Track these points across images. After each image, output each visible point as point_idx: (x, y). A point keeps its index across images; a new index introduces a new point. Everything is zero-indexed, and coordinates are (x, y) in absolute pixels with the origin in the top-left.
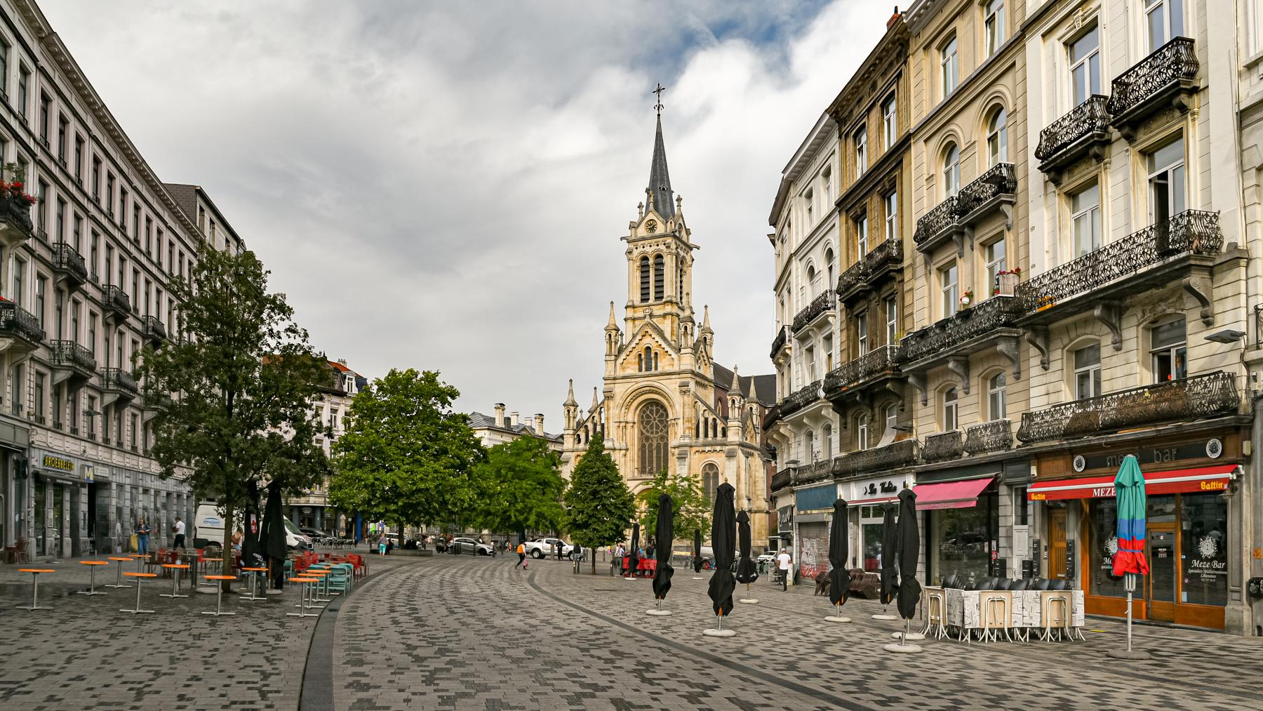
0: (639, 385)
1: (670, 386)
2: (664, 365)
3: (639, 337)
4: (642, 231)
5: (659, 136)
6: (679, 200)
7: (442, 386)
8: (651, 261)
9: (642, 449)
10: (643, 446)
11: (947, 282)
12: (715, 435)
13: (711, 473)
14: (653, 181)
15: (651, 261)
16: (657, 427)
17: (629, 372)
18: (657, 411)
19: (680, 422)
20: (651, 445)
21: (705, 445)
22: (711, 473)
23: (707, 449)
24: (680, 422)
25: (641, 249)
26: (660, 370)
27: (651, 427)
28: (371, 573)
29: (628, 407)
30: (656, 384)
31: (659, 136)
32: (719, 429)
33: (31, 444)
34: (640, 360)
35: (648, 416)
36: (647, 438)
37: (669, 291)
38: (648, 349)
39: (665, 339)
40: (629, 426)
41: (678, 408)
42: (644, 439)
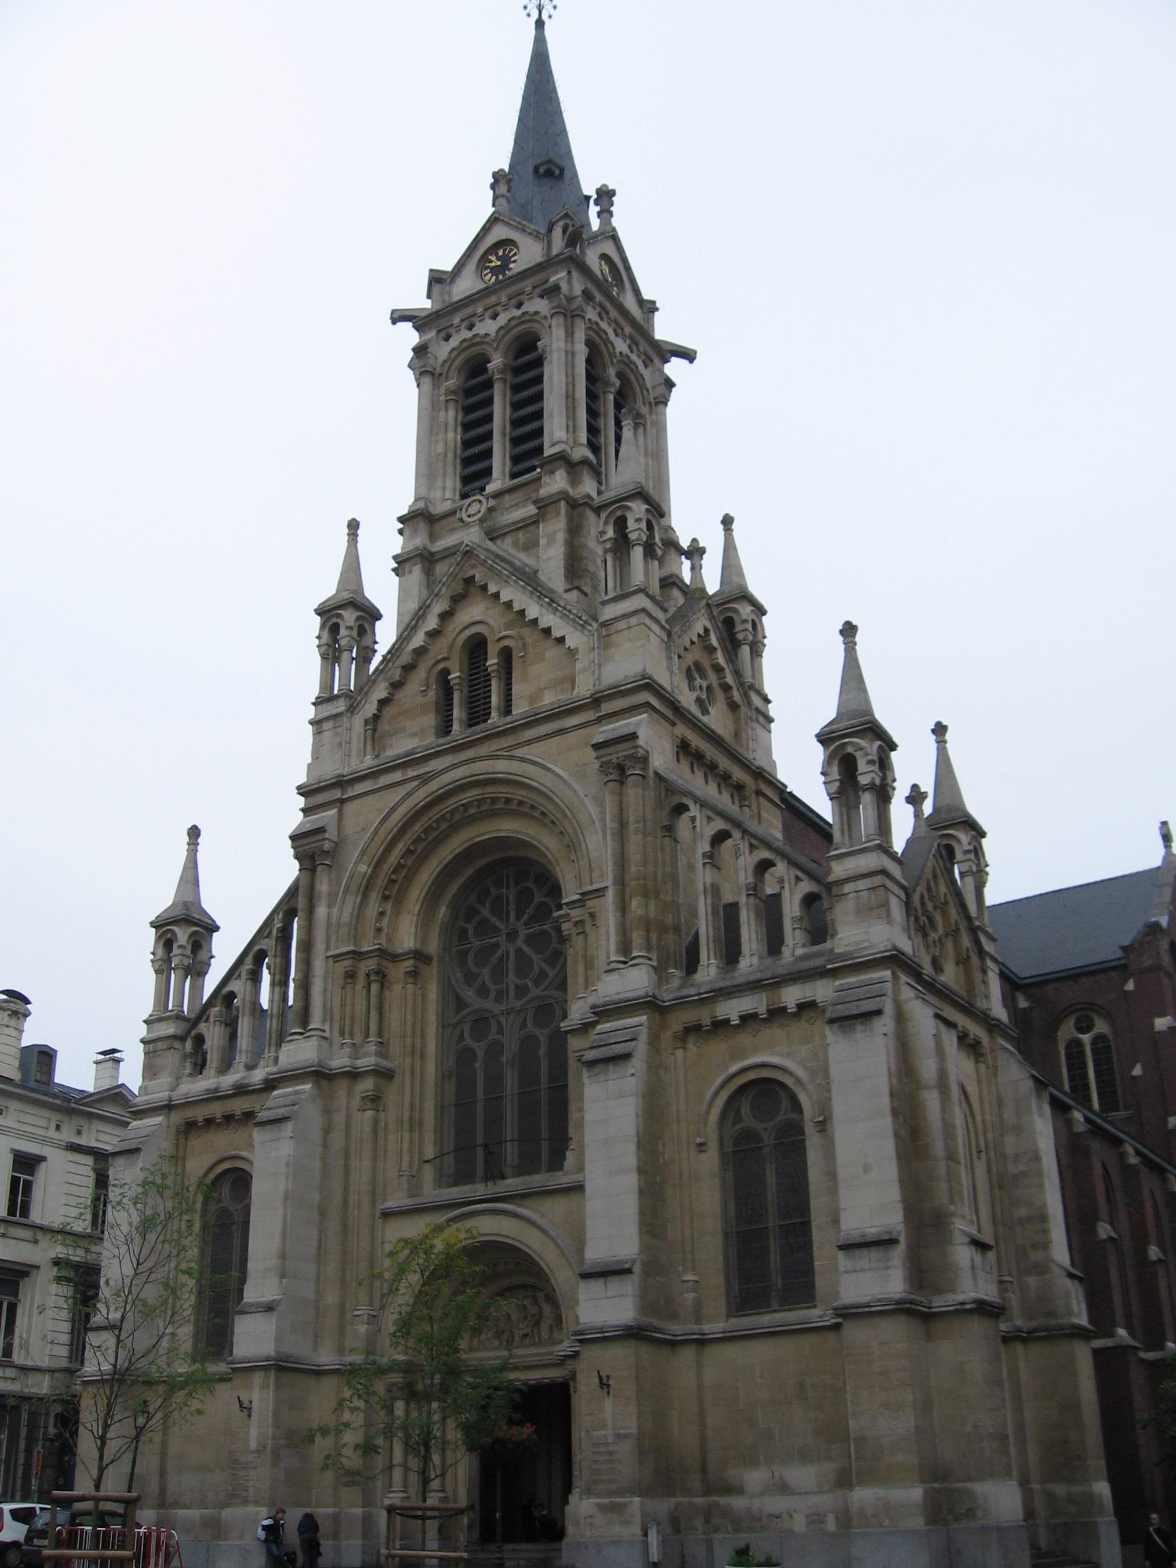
1: (561, 767)
2: (534, 687)
9: (459, 1070)
10: (465, 1058)
11: (600, 483)
12: (774, 943)
13: (767, 1131)
17: (400, 746)
18: (524, 897)
19: (608, 906)
20: (495, 1050)
22: (767, 1131)
24: (608, 906)
26: (520, 709)
27: (499, 972)
28: (335, 838)
29: (395, 891)
30: (502, 766)
34: (447, 690)
36: (481, 1023)
40: (398, 972)
41: (598, 845)
42: (466, 1026)
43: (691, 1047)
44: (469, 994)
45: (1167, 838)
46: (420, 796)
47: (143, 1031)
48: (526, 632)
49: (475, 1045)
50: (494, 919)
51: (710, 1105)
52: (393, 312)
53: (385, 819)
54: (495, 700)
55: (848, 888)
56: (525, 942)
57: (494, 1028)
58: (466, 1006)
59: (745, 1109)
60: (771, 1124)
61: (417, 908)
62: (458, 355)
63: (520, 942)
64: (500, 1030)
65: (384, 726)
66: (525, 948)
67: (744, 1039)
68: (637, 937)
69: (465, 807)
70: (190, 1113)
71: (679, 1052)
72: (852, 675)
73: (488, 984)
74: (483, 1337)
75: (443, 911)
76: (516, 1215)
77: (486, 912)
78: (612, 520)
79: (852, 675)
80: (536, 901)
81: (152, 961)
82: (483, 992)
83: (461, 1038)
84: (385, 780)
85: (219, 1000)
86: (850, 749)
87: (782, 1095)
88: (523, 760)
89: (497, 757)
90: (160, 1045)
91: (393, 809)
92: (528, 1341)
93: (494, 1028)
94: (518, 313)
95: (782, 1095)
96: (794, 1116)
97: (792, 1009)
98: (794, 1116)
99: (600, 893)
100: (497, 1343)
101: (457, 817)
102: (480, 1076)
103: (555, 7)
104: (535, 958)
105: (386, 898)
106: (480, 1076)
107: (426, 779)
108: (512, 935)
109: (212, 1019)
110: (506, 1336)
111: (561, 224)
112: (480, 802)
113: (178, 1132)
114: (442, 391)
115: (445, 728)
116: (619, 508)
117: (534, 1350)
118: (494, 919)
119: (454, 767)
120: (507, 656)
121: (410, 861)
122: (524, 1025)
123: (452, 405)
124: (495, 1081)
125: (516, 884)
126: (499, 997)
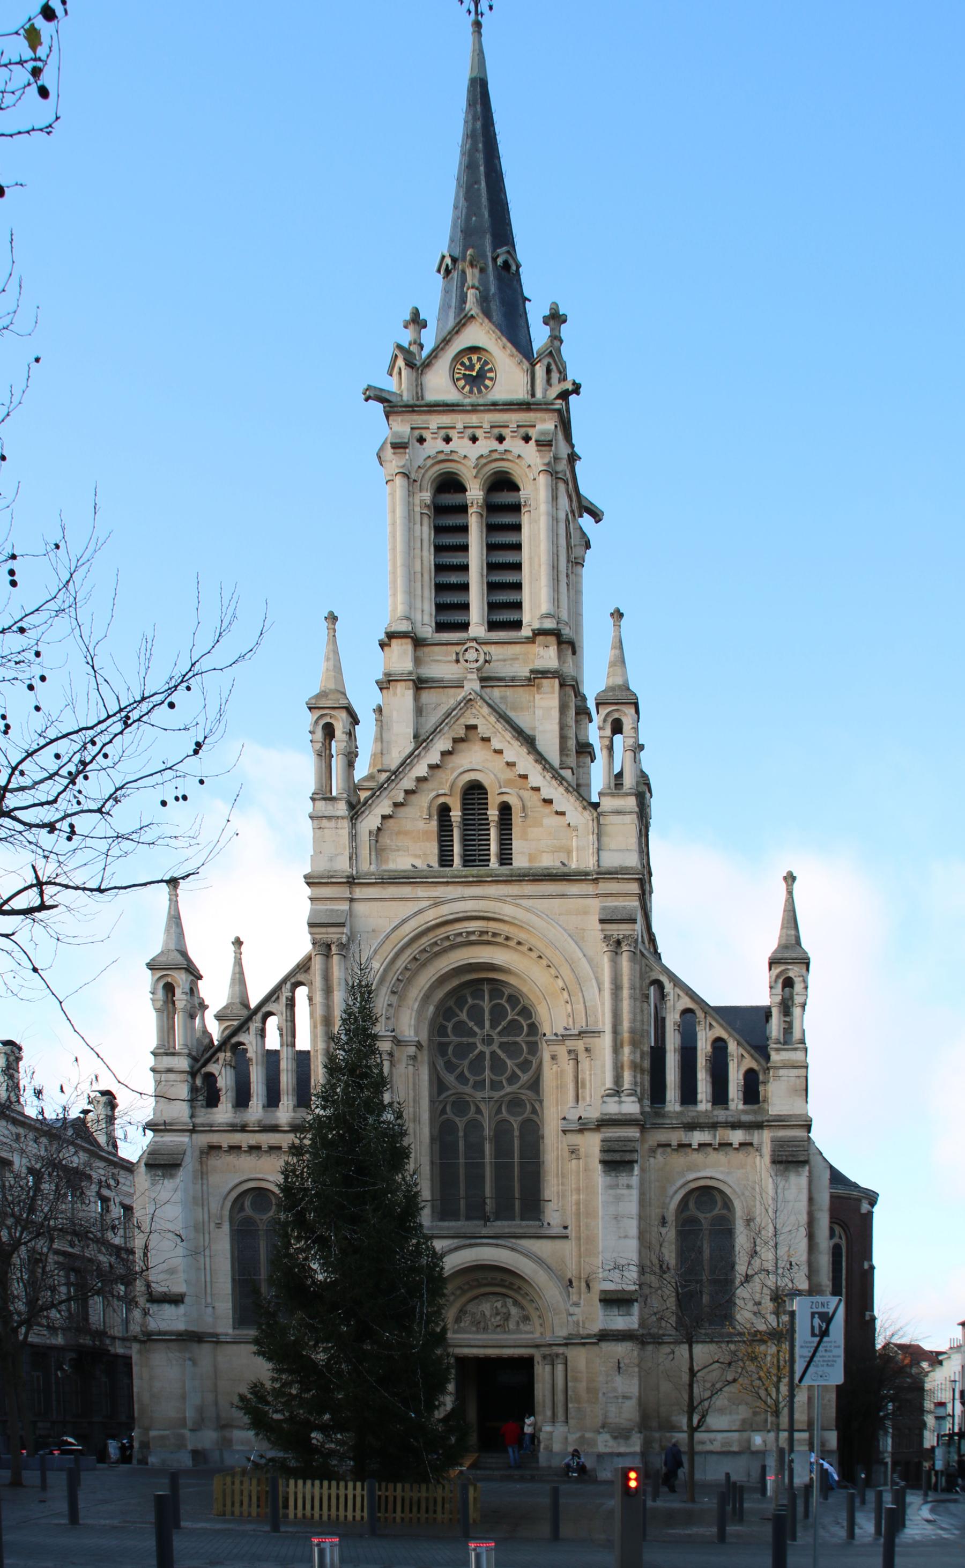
0: (445, 911)
3: (444, 743)
4: (440, 384)
5: (480, 93)
6: (555, 318)
7: (91, 1302)
8: (475, 493)
14: (467, 232)
15: (475, 493)
16: (498, 1065)
17: (401, 862)
21: (691, 1127)
22: (705, 1218)
23: (698, 1137)
25: (434, 445)
30: (507, 910)
31: (480, 93)
32: (735, 1078)
33: (926, 1502)
35: (460, 1028)
37: (536, 603)
38: (474, 793)
39: (541, 758)
43: (659, 1156)
44: (450, 1079)
45: (63, 529)
46: (432, 916)
47: (151, 1061)
48: (527, 794)
49: (457, 1119)
50: (471, 1024)
51: (672, 1198)
52: (369, 388)
53: (396, 928)
54: (494, 847)
55: (782, 1072)
56: (499, 1047)
57: (473, 1109)
58: (448, 1089)
59: (691, 1205)
60: (708, 1215)
61: (416, 1006)
62: (433, 465)
63: (495, 1047)
64: (479, 1111)
65: (385, 840)
66: (499, 1052)
67: (697, 1157)
68: (627, 1076)
69: (469, 933)
70: (215, 1139)
71: (652, 1160)
72: (791, 919)
73: (466, 1073)
74: (462, 1325)
75: (431, 1009)
76: (513, 1249)
77: (463, 1016)
78: (610, 720)
79: (791, 919)
80: (509, 1018)
81: (153, 1000)
82: (462, 1078)
83: (443, 1111)
84: (392, 891)
85: (229, 1047)
86: (791, 974)
87: (715, 1193)
88: (527, 910)
89: (505, 902)
90: (172, 1076)
91: (404, 921)
92: (499, 1329)
93: (473, 1109)
94: (495, 445)
95: (715, 1193)
96: (724, 1212)
97: (736, 1145)
98: (724, 1212)
99: (597, 1033)
100: (474, 1329)
101: (459, 939)
102: (461, 1144)
103: (491, 8)
104: (509, 1062)
105: (393, 992)
106: (461, 1144)
107: (437, 903)
108: (489, 1041)
109: (221, 1062)
110: (482, 1324)
111: (545, 361)
112: (482, 933)
113: (202, 1152)
114: (417, 502)
115: (445, 859)
116: (617, 710)
117: (484, 1336)
118: (471, 1024)
119: (463, 899)
120: (505, 809)
121: (413, 966)
122: (499, 1111)
123: (426, 520)
124: (475, 1149)
125: (491, 1000)
126: (479, 1085)
